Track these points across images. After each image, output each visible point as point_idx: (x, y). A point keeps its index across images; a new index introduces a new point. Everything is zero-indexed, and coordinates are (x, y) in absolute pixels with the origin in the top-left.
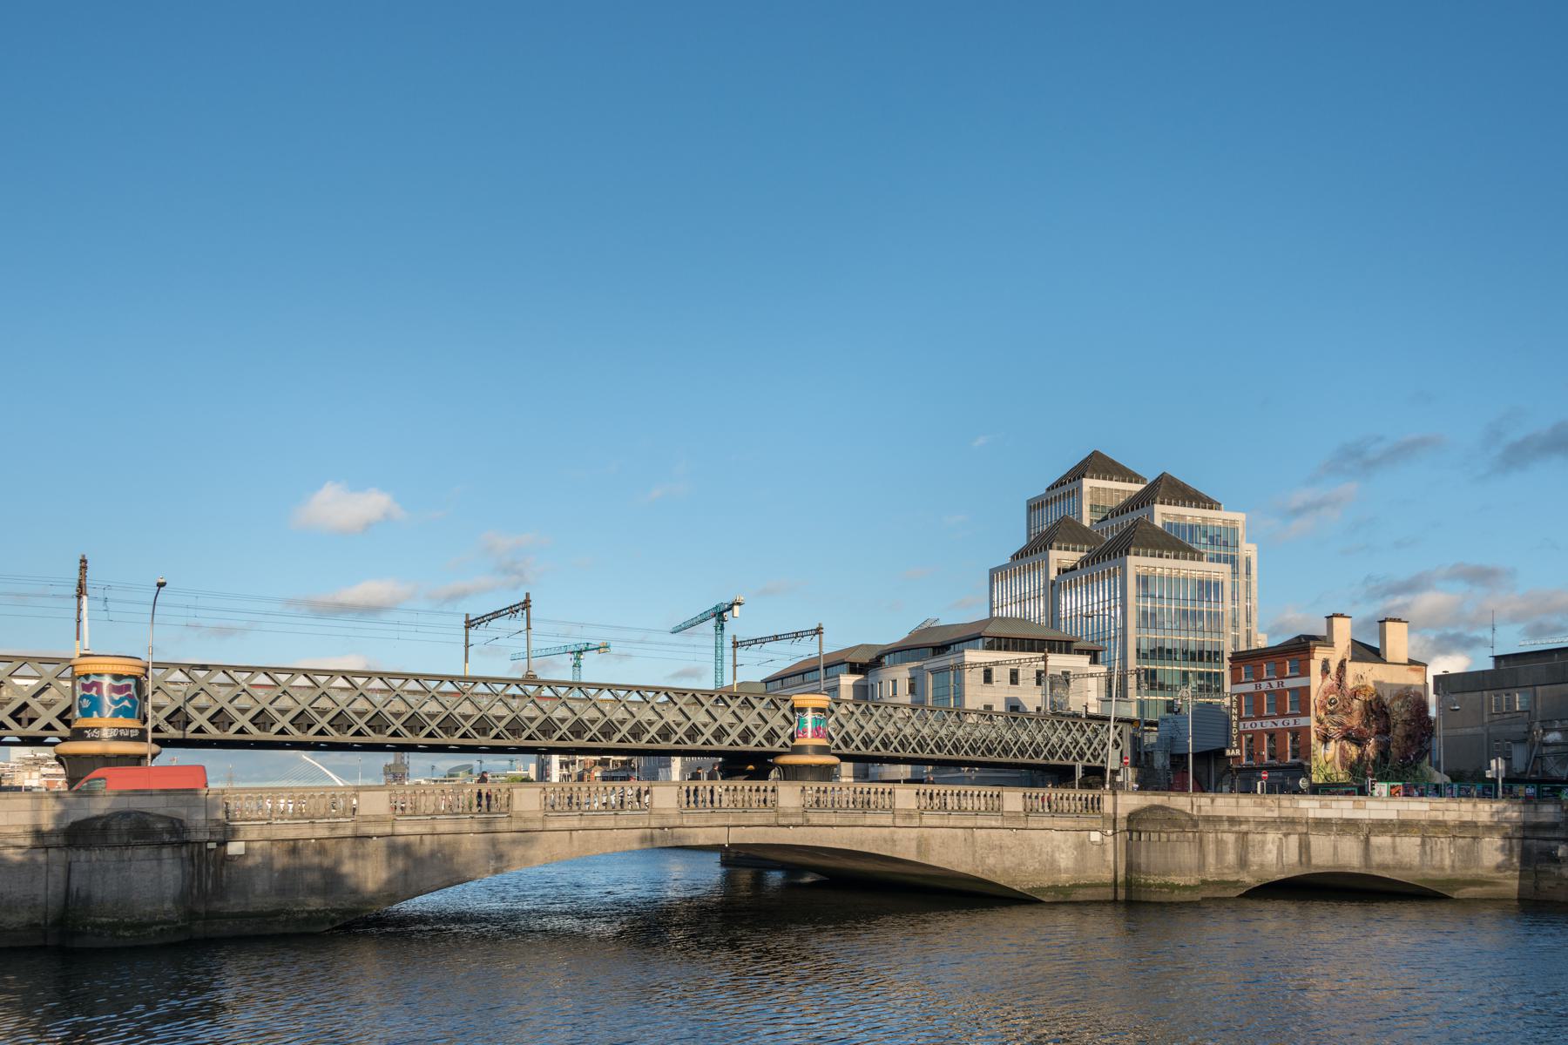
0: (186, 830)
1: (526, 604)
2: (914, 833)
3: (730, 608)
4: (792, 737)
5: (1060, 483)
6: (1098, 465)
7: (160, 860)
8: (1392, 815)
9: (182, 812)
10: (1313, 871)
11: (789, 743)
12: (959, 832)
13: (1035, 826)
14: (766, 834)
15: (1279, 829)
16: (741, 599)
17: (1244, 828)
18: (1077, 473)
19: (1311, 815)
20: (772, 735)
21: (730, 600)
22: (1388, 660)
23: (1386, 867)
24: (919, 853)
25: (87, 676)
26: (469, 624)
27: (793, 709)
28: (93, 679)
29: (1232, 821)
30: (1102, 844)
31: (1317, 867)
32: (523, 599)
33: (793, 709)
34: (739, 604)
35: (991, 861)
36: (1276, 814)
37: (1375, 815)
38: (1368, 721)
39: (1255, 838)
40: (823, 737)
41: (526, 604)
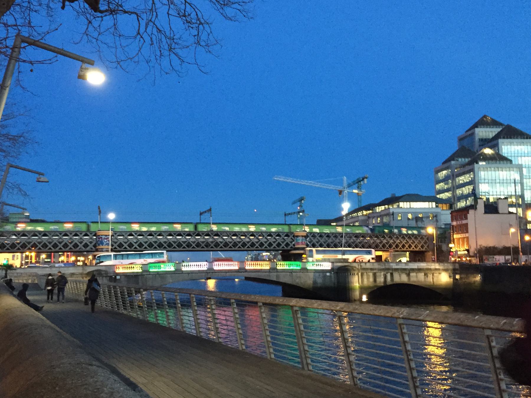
0: (108, 273)
1: (210, 210)
2: (275, 274)
3: (363, 180)
4: (294, 245)
5: (470, 130)
6: (482, 123)
7: (103, 279)
8: (416, 267)
9: (108, 270)
10: (394, 283)
11: (293, 247)
12: (288, 273)
13: (223, 273)
14: (218, 275)
15: (384, 271)
16: (367, 176)
17: (375, 271)
18: (476, 126)
19: (394, 267)
20: (287, 245)
21: (363, 176)
22: (500, 212)
23: (415, 282)
24: (277, 279)
25: (99, 236)
26: (201, 214)
27: (294, 236)
28: (101, 236)
29: (371, 269)
30: (330, 276)
31: (396, 282)
32: (209, 208)
33: (294, 236)
34: (367, 178)
35: (297, 281)
36: (384, 267)
37: (411, 267)
38: (33, 276)
39: (378, 274)
40: (303, 245)
41: (210, 210)
